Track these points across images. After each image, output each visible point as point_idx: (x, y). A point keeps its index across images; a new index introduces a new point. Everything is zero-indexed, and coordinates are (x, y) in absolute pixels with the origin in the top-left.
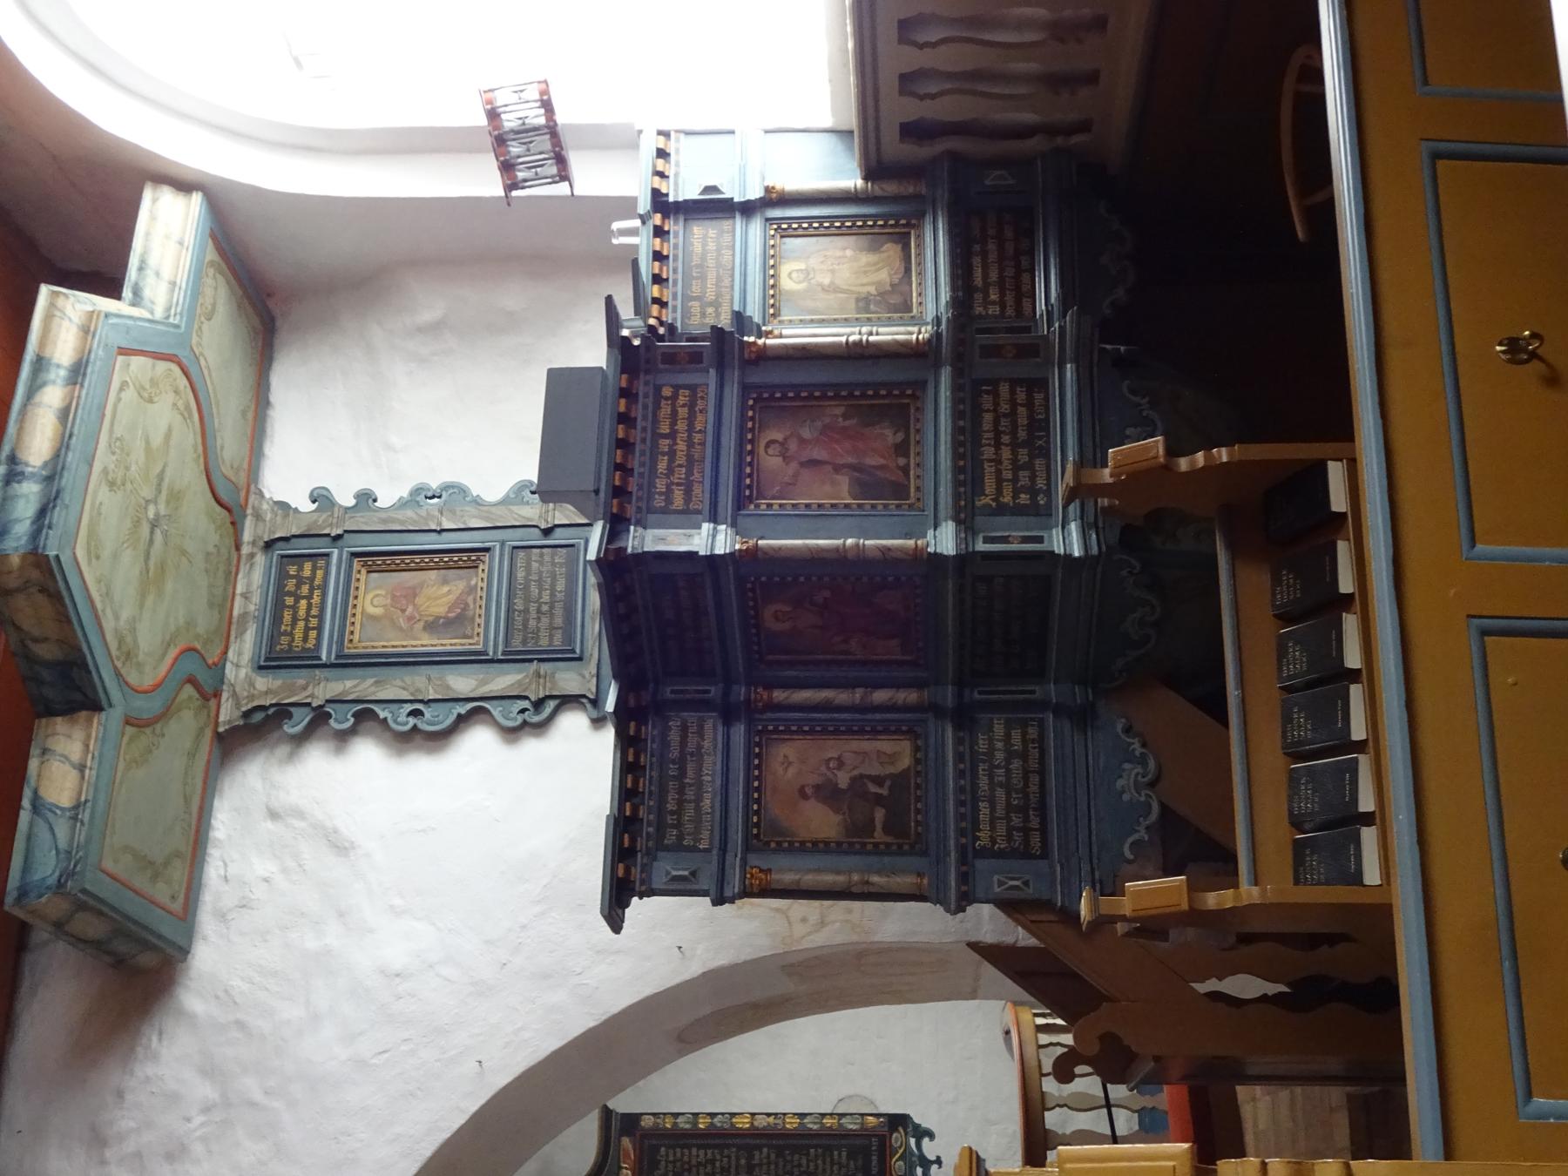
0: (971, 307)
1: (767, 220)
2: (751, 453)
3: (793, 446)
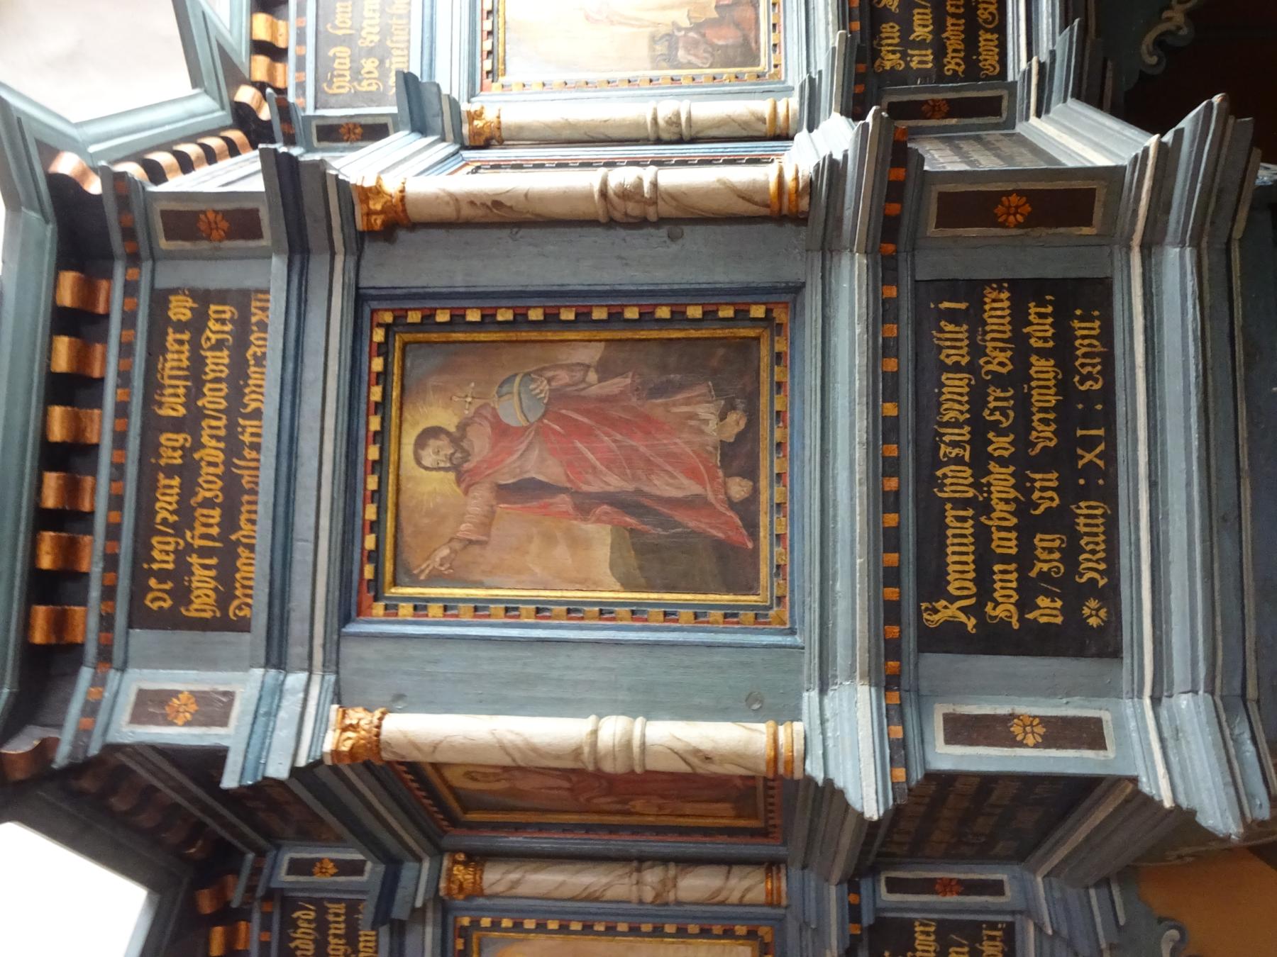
0: (876, 54)
2: (379, 466)
3: (480, 443)
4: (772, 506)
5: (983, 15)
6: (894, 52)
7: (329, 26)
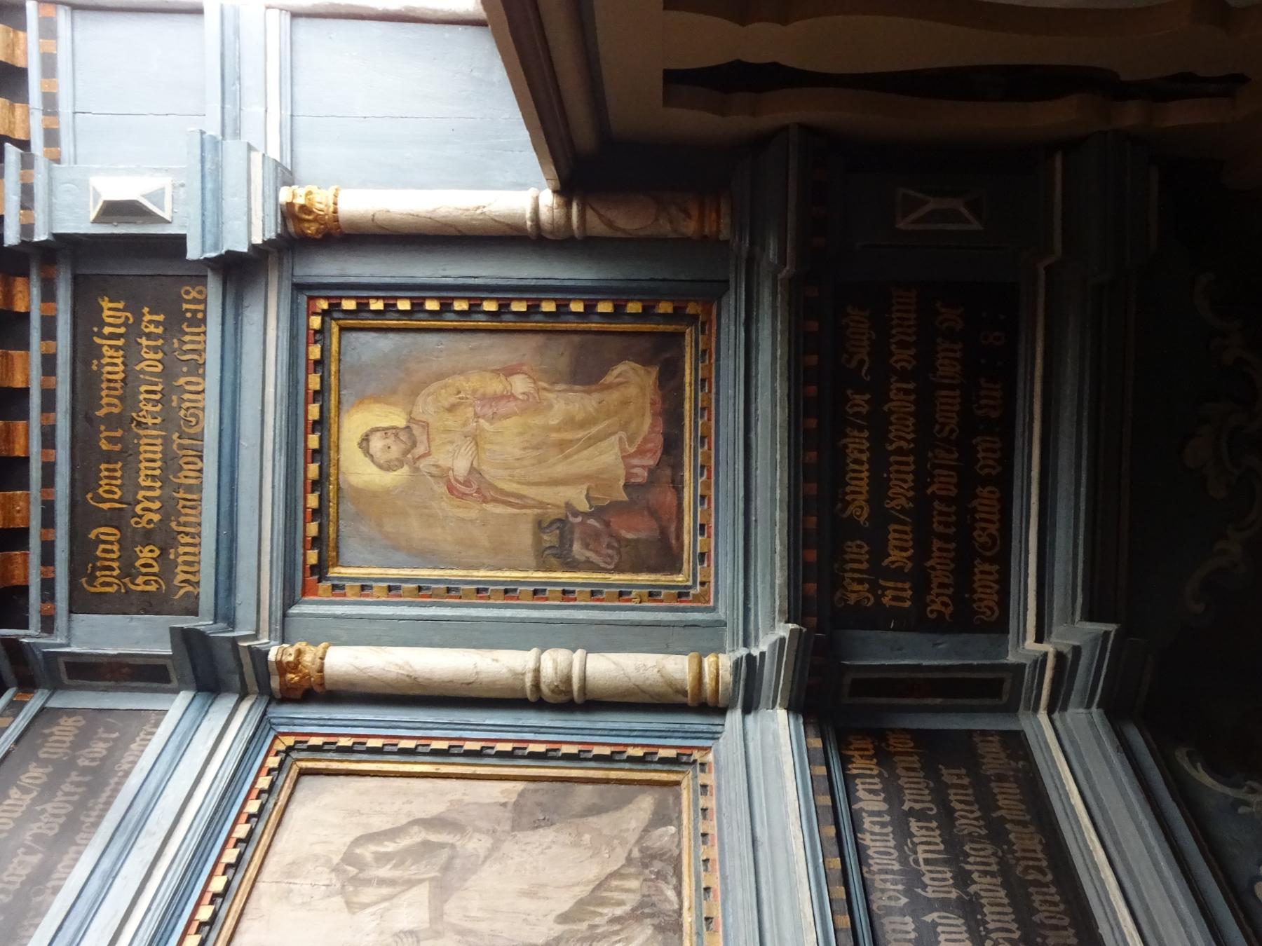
1: (298, 288)
4: (696, 837)
5: (980, 537)
6: (860, 581)
7: (89, 496)
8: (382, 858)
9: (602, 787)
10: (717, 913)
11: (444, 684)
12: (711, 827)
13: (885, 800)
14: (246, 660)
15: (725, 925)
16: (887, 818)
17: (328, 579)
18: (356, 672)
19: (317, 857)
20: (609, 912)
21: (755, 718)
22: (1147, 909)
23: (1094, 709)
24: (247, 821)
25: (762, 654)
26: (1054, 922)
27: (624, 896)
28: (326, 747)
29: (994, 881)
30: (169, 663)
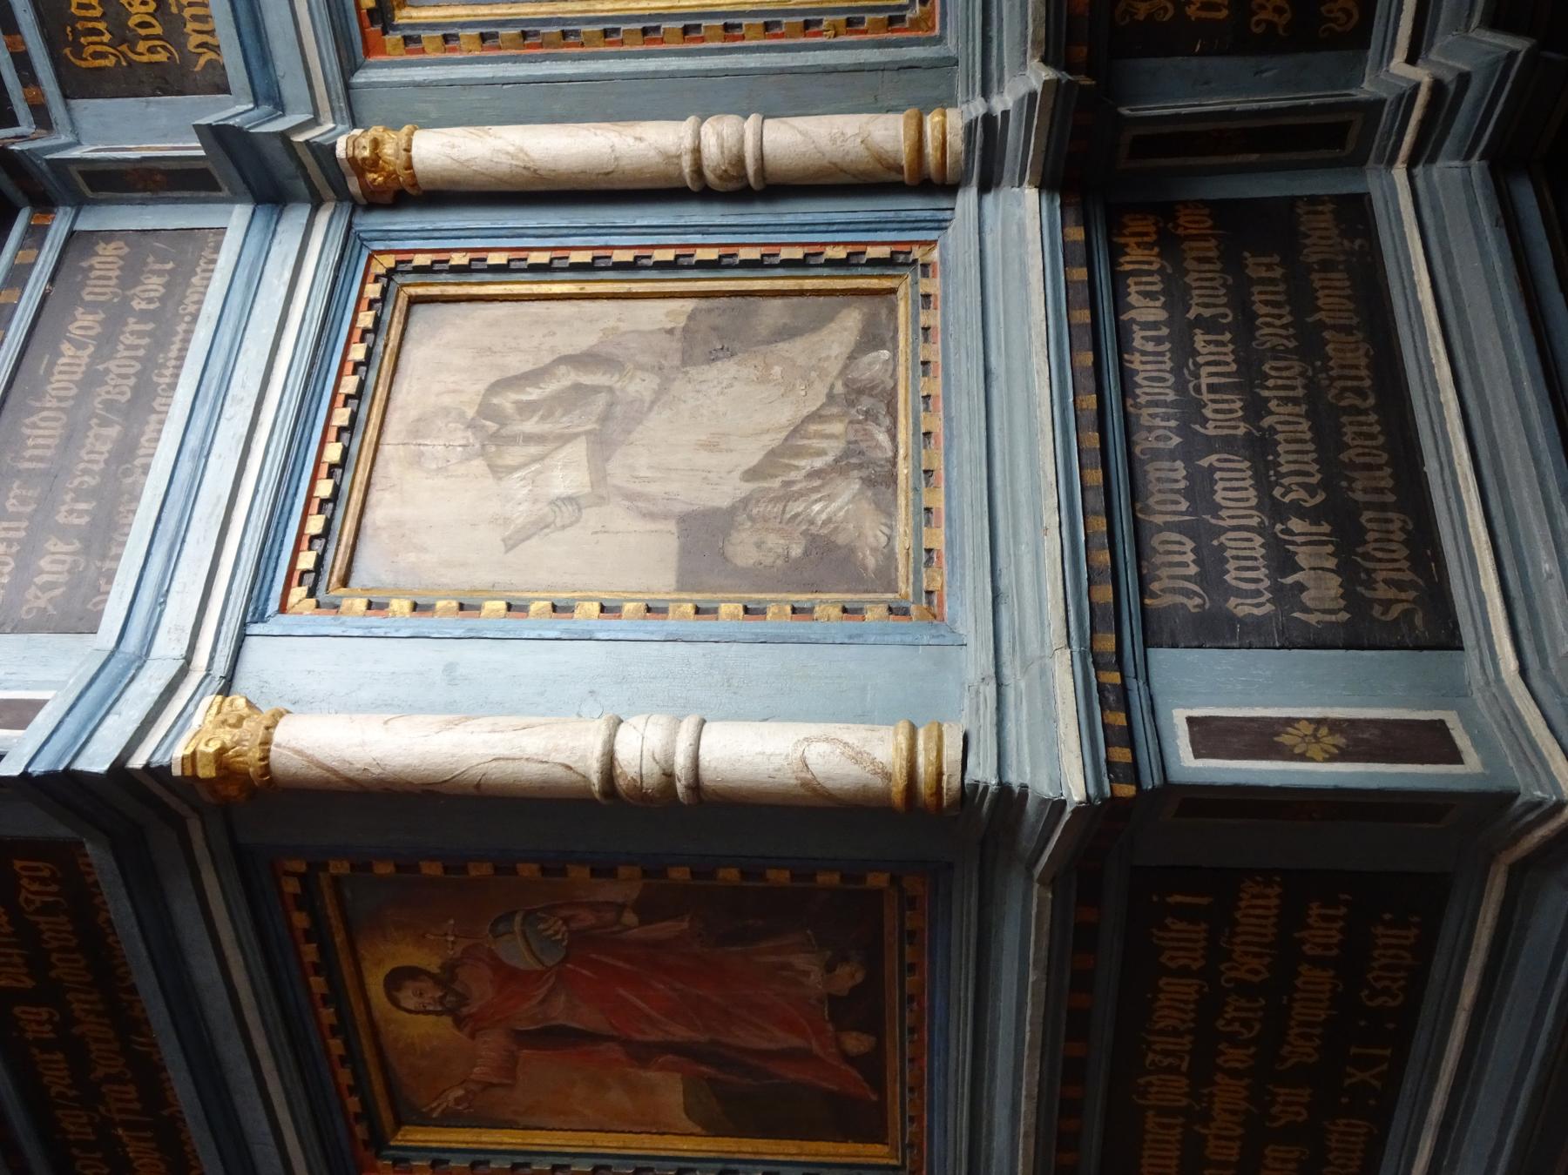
3: (480, 989)
4: (914, 365)
8: (526, 409)
9: (795, 300)
10: (938, 464)
11: (572, 176)
12: (933, 352)
13: (1164, 307)
14: (308, 159)
15: (947, 480)
16: (1165, 331)
17: (396, 28)
18: (456, 166)
19: (446, 411)
20: (806, 464)
21: (996, 198)
22: (1492, 443)
23: (1474, 161)
24: (355, 372)
25: (1005, 113)
26: (1368, 459)
27: (824, 444)
28: (437, 267)
29: (1297, 410)
30: (209, 165)
